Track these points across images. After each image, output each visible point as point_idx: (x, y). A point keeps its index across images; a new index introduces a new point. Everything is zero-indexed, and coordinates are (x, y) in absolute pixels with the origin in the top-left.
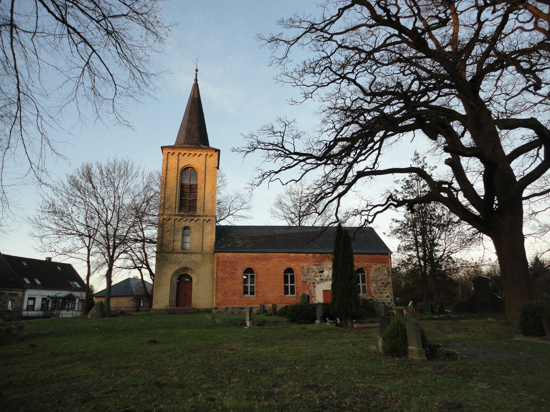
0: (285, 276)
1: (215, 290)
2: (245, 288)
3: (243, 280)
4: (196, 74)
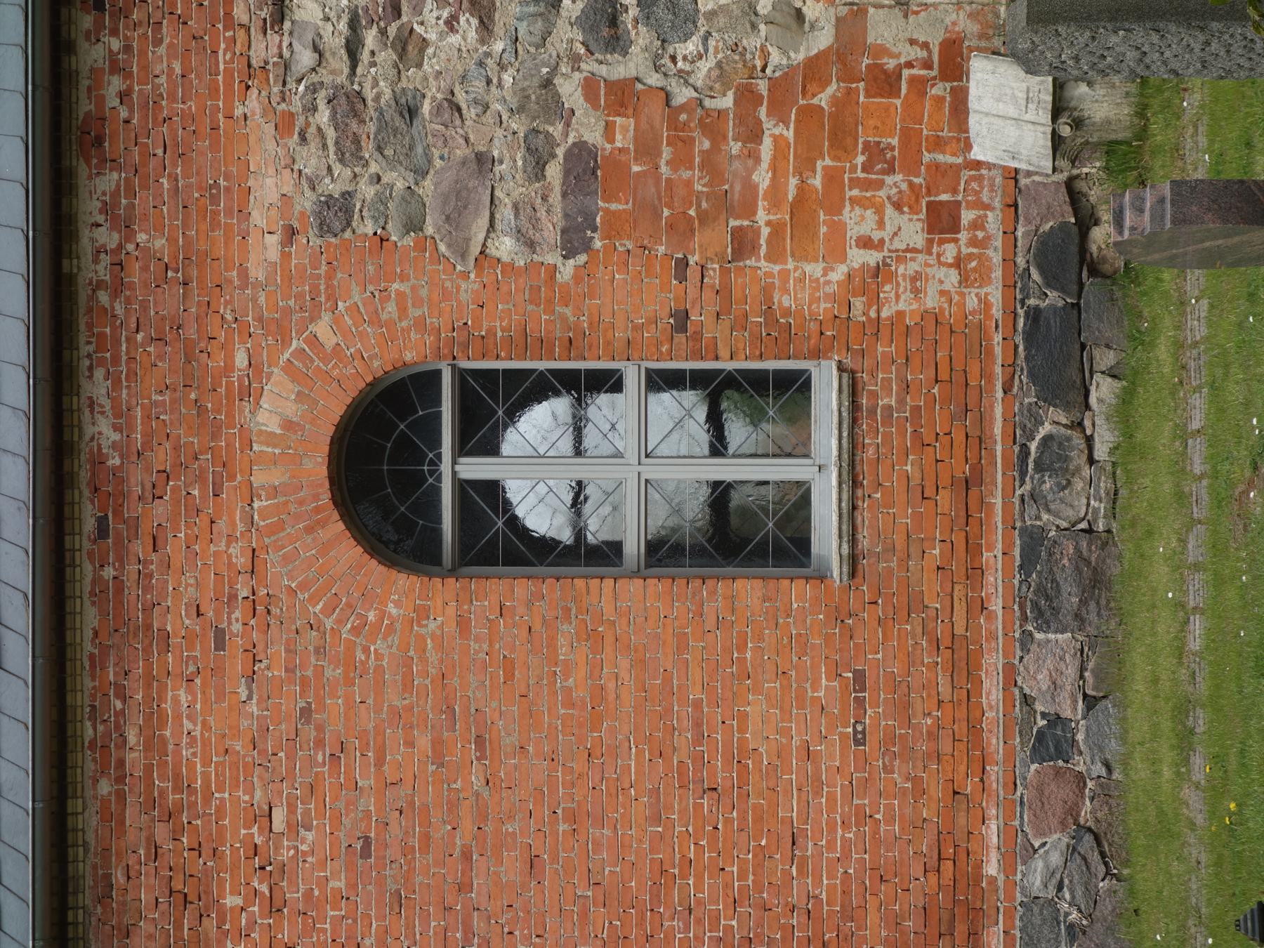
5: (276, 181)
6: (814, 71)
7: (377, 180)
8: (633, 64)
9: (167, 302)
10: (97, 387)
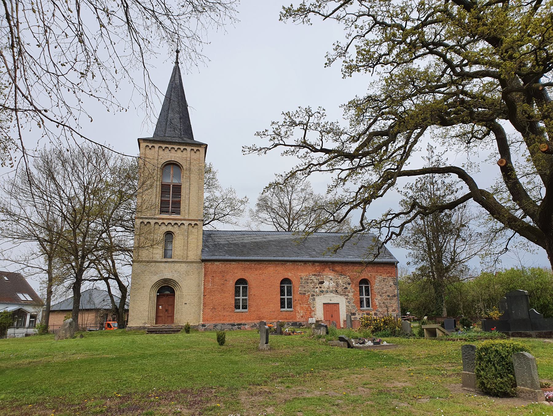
1: (202, 305)
2: (237, 301)
5: (303, 275)
6: (311, 309)
7: (304, 281)
8: (311, 297)
9: (296, 268)
10: (291, 263)
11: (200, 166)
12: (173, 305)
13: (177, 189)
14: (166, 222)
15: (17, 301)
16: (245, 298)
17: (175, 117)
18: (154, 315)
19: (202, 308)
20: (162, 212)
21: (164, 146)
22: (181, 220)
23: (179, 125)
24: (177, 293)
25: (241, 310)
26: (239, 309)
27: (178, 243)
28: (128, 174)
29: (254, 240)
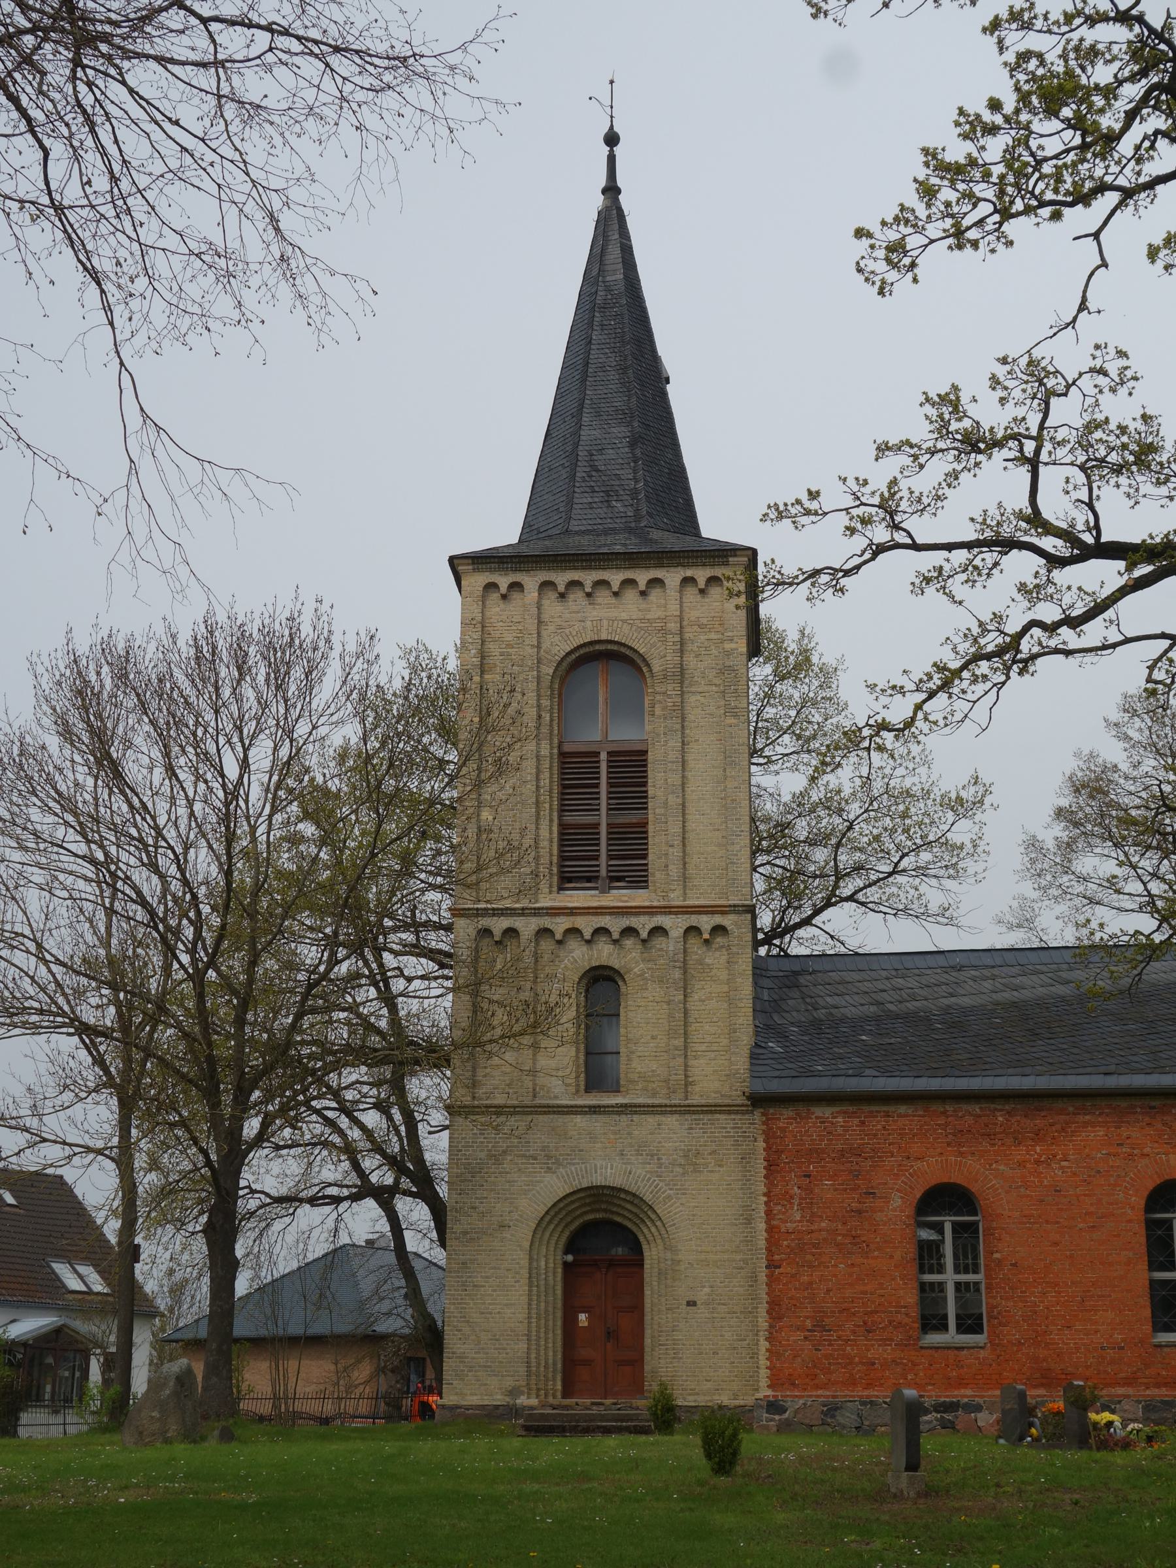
0: (1151, 1225)
1: (763, 1309)
2: (930, 1294)
3: (912, 1251)
4: (612, 159)
11: (728, 654)
12: (637, 1308)
13: (631, 767)
14: (587, 925)
15: (47, 1293)
16: (970, 1277)
17: (610, 439)
18: (553, 1352)
19: (763, 1322)
20: (566, 880)
21: (561, 578)
22: (650, 911)
23: (626, 473)
24: (652, 1254)
25: (951, 1336)
26: (944, 1327)
27: (643, 1018)
28: (420, 718)
29: (1007, 995)
